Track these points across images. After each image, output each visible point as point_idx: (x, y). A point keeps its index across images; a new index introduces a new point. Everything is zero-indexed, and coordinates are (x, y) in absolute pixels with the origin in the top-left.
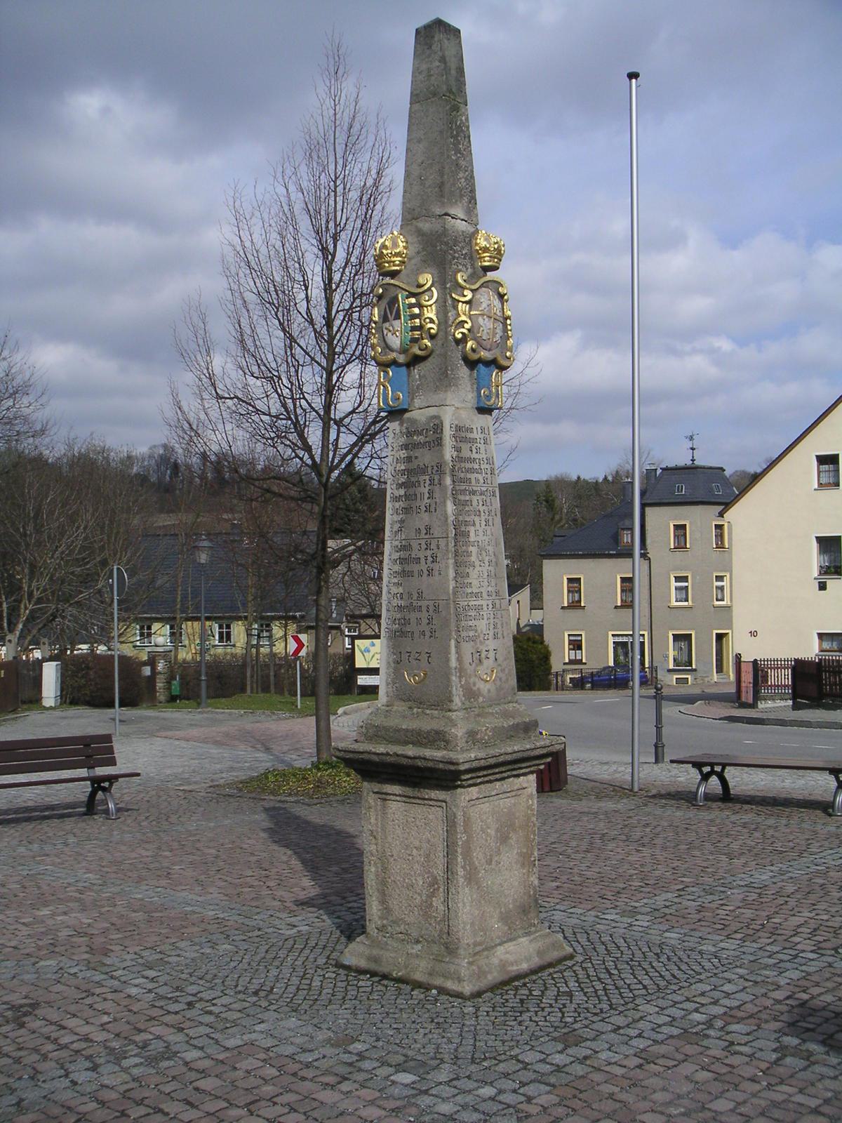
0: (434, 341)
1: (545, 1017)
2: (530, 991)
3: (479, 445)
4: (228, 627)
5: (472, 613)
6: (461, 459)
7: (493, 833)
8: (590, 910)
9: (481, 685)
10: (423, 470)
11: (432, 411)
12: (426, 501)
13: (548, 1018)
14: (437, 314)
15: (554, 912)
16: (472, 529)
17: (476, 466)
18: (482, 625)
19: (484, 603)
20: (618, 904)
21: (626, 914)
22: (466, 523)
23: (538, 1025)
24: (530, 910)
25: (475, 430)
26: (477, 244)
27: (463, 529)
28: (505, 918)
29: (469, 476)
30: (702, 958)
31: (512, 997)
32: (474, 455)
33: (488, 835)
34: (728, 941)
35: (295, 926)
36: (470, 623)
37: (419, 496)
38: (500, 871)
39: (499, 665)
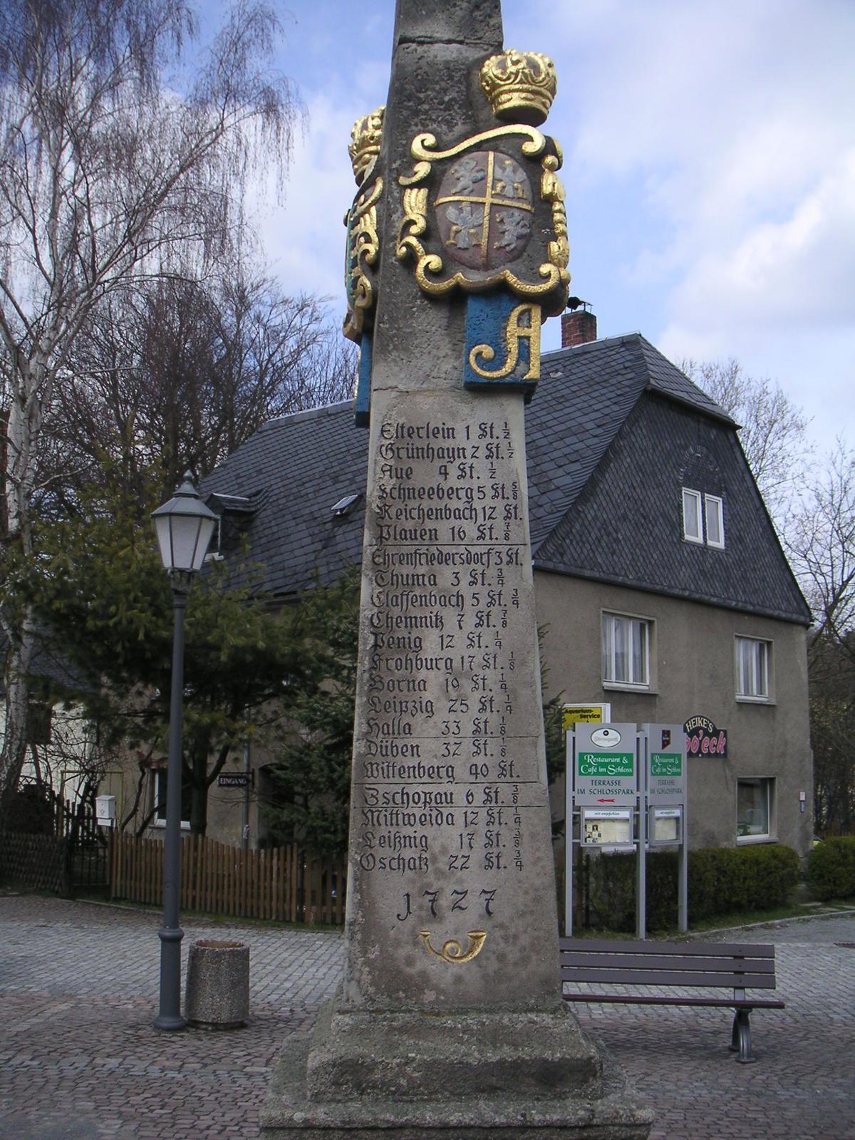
3: (469, 461)
6: (406, 493)
22: (412, 622)
26: (483, 76)
29: (429, 525)
32: (453, 481)
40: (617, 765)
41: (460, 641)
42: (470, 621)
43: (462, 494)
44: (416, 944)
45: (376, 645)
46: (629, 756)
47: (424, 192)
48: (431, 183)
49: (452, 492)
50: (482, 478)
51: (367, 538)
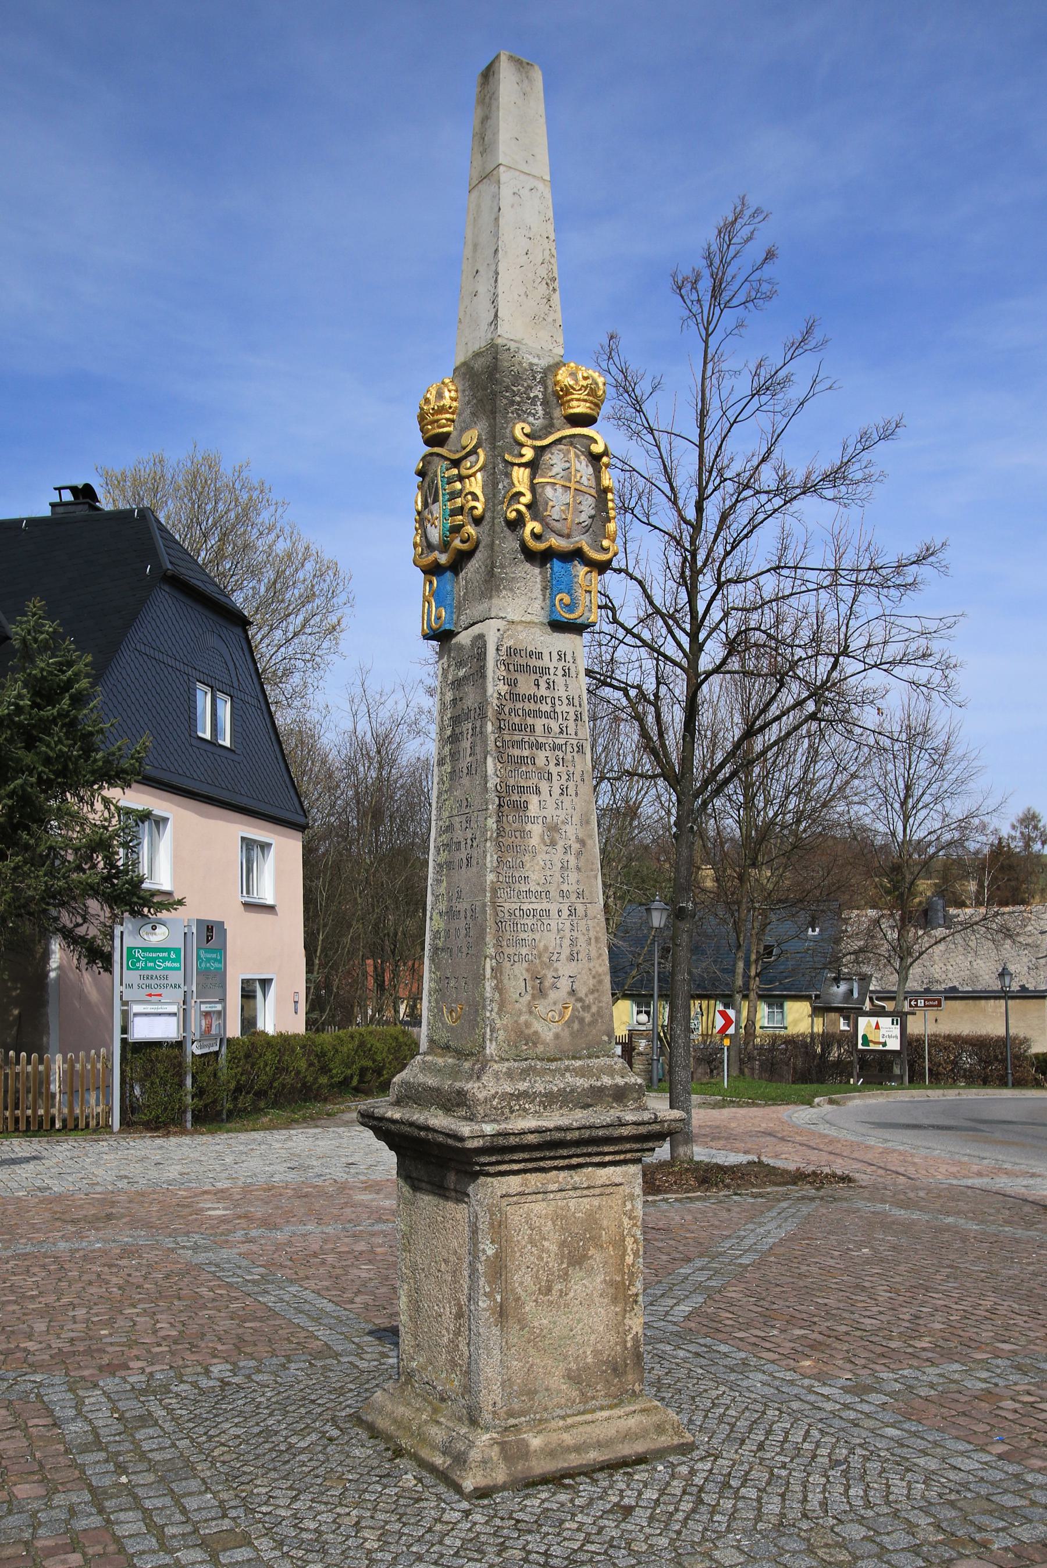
0: (480, 529)
3: (552, 677)
6: (514, 697)
7: (554, 1248)
9: (537, 1026)
14: (484, 487)
16: (534, 800)
19: (554, 908)
24: (624, 1371)
25: (546, 657)
26: (556, 383)
28: (573, 1378)
29: (530, 721)
32: (543, 691)
38: (567, 1305)
40: (164, 960)
41: (550, 803)
42: (556, 791)
43: (549, 700)
44: (531, 1012)
45: (500, 805)
46: (177, 951)
47: (528, 471)
48: (533, 466)
49: (543, 698)
50: (561, 692)
51: (490, 728)
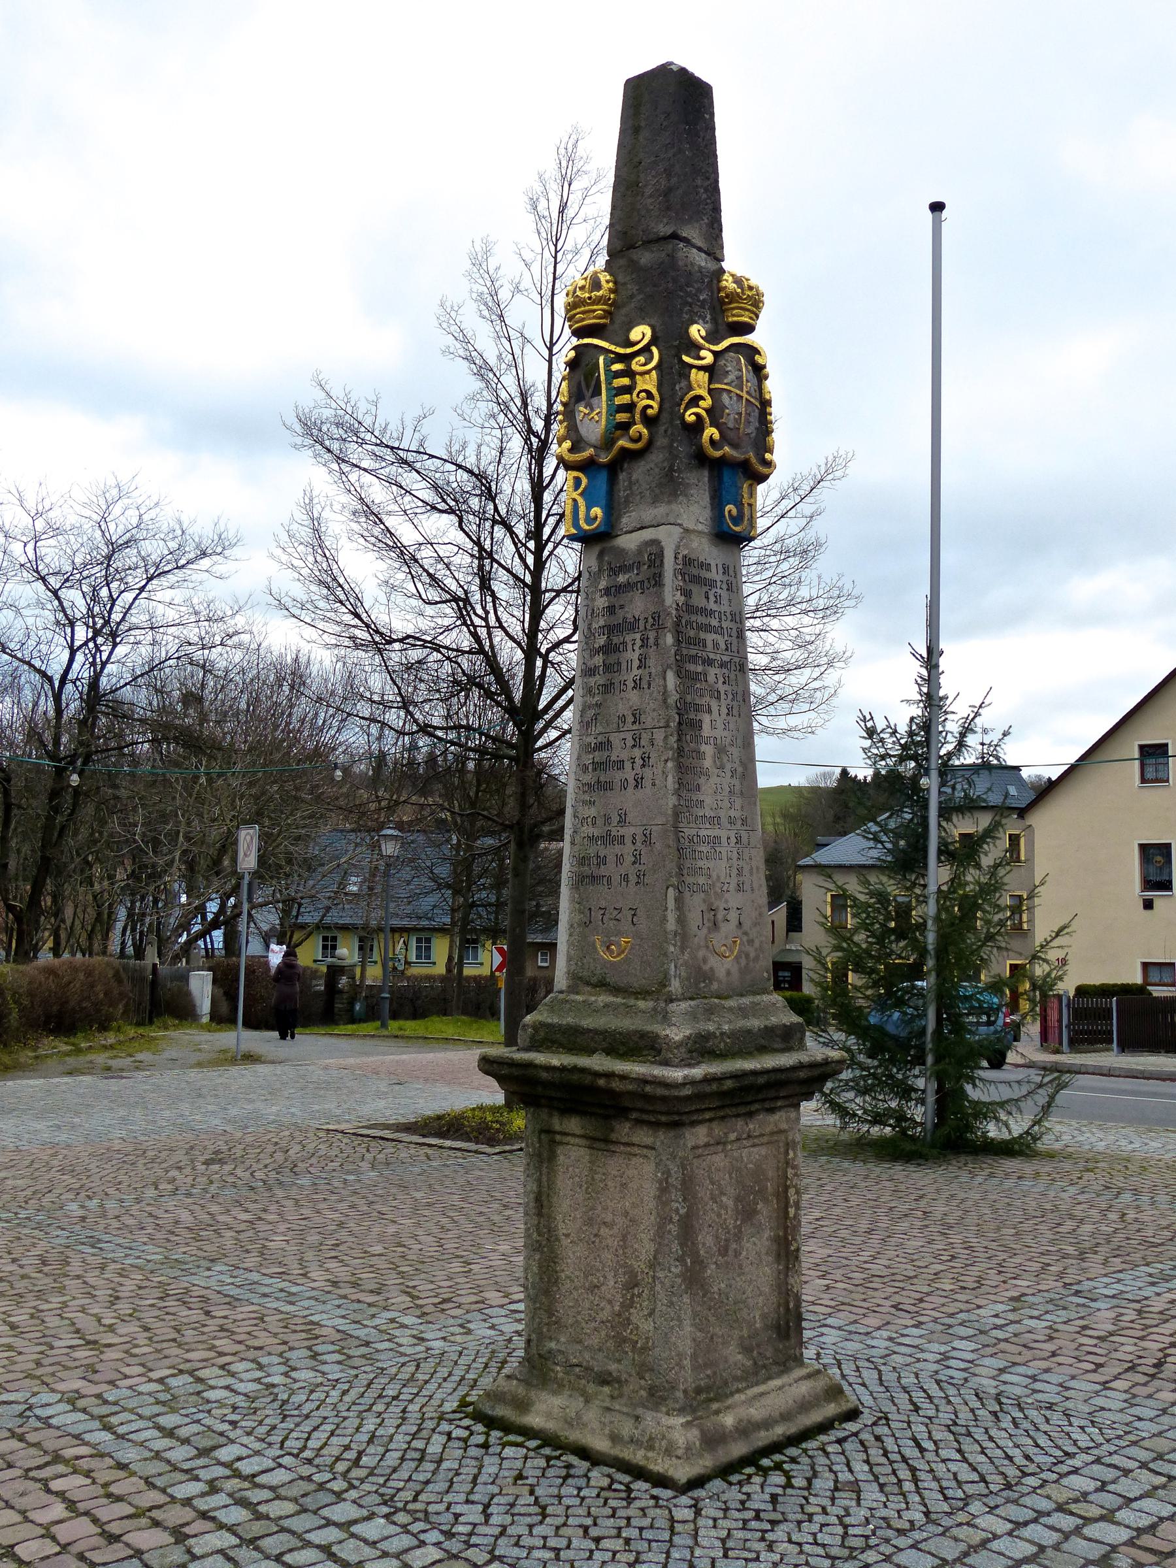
1: (815, 1535)
2: (789, 1478)
4: (428, 940)
5: (704, 848)
6: (690, 609)
7: (730, 1203)
8: (879, 1328)
10: (632, 626)
11: (647, 534)
12: (635, 672)
13: (819, 1536)
15: (824, 1330)
16: (706, 719)
17: (714, 623)
18: (720, 868)
19: (723, 834)
20: (921, 1319)
21: (935, 1336)
22: (698, 708)
23: (801, 1552)
25: (714, 569)
27: (692, 716)
29: (702, 635)
30: (1071, 1425)
31: (758, 1488)
32: (712, 606)
33: (724, 1207)
34: (1109, 1393)
35: (423, 1339)
36: (700, 863)
37: (624, 666)
39: (746, 933)
42: (724, 711)
45: (680, 723)
49: (712, 612)
